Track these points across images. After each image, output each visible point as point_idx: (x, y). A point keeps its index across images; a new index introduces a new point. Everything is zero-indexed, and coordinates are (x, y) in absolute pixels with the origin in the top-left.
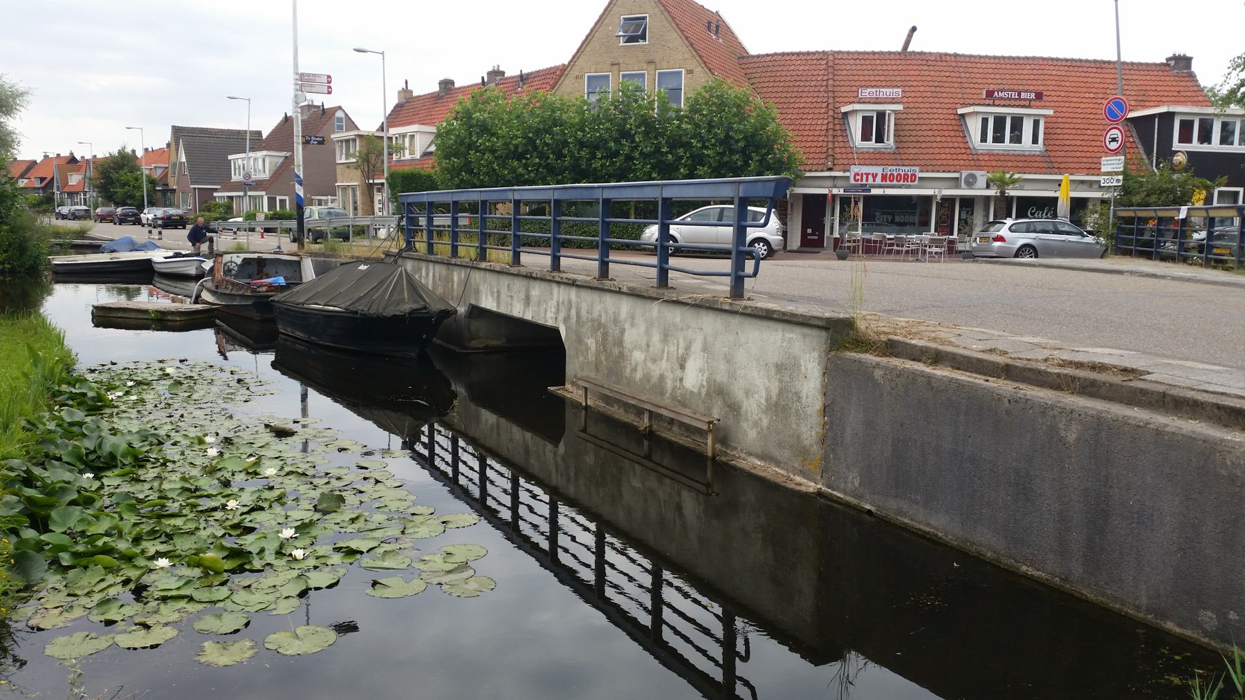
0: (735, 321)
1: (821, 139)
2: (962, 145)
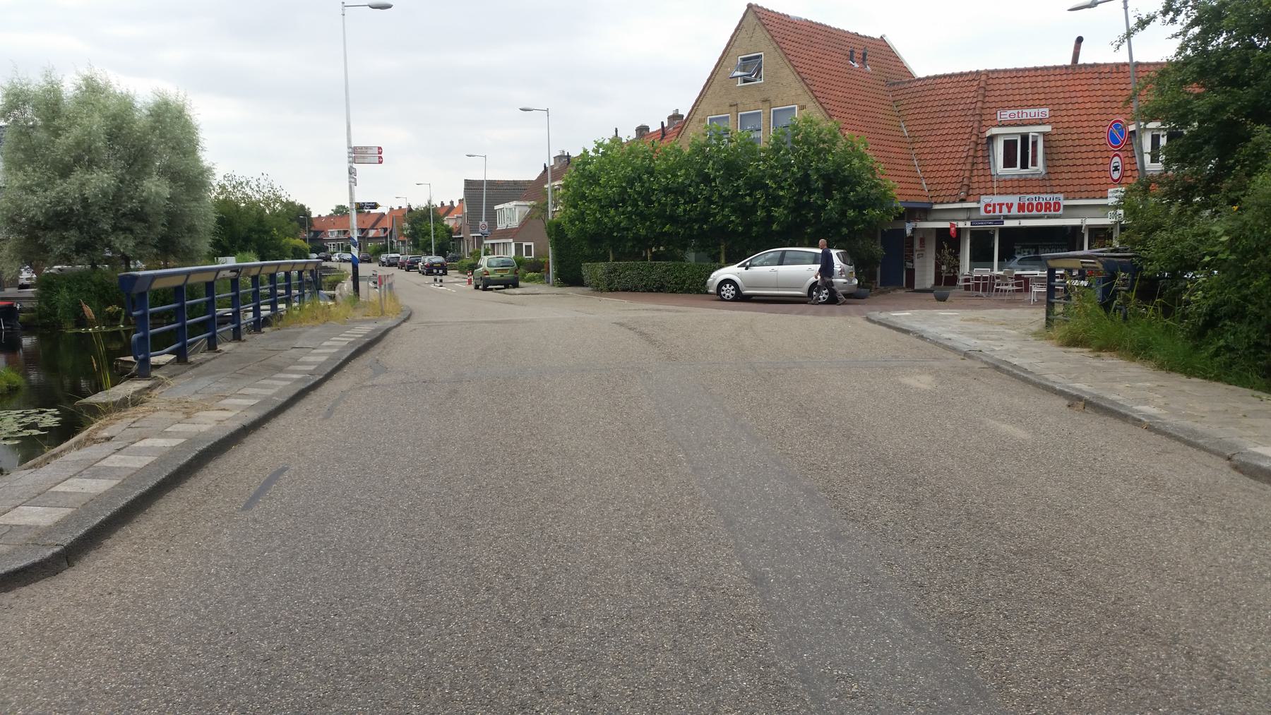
1: (959, 167)
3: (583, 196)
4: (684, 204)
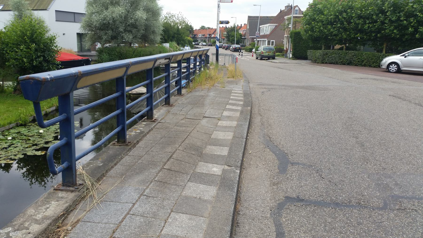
3: (314, 20)
4: (368, 23)
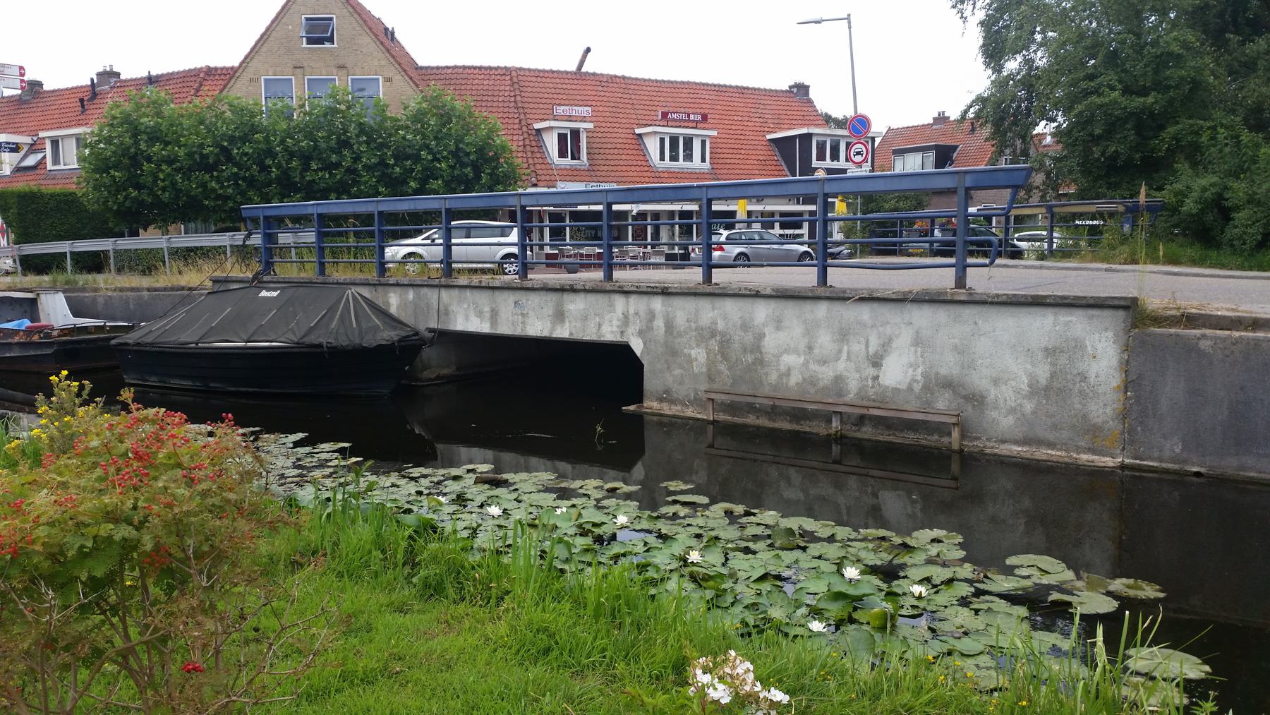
0: (968, 312)
2: (644, 163)
